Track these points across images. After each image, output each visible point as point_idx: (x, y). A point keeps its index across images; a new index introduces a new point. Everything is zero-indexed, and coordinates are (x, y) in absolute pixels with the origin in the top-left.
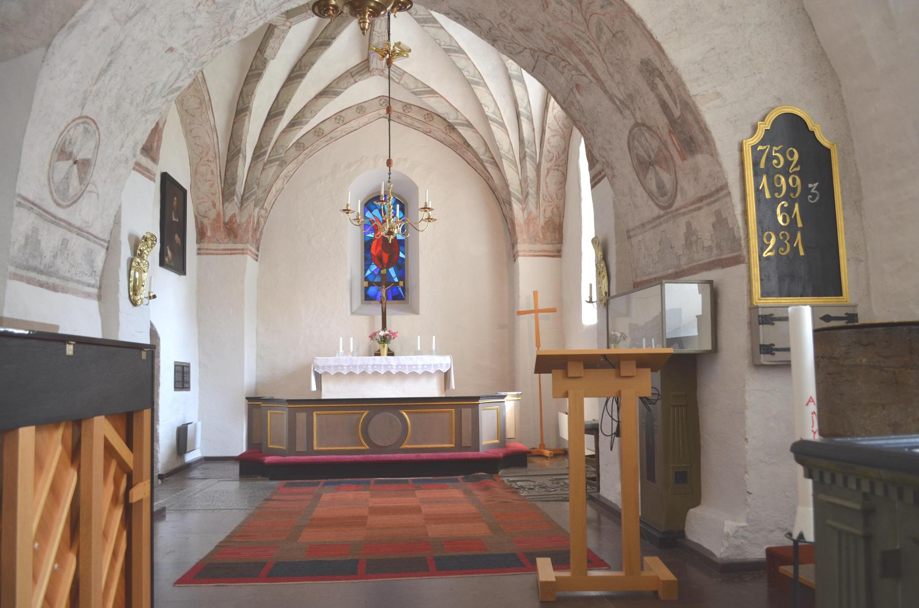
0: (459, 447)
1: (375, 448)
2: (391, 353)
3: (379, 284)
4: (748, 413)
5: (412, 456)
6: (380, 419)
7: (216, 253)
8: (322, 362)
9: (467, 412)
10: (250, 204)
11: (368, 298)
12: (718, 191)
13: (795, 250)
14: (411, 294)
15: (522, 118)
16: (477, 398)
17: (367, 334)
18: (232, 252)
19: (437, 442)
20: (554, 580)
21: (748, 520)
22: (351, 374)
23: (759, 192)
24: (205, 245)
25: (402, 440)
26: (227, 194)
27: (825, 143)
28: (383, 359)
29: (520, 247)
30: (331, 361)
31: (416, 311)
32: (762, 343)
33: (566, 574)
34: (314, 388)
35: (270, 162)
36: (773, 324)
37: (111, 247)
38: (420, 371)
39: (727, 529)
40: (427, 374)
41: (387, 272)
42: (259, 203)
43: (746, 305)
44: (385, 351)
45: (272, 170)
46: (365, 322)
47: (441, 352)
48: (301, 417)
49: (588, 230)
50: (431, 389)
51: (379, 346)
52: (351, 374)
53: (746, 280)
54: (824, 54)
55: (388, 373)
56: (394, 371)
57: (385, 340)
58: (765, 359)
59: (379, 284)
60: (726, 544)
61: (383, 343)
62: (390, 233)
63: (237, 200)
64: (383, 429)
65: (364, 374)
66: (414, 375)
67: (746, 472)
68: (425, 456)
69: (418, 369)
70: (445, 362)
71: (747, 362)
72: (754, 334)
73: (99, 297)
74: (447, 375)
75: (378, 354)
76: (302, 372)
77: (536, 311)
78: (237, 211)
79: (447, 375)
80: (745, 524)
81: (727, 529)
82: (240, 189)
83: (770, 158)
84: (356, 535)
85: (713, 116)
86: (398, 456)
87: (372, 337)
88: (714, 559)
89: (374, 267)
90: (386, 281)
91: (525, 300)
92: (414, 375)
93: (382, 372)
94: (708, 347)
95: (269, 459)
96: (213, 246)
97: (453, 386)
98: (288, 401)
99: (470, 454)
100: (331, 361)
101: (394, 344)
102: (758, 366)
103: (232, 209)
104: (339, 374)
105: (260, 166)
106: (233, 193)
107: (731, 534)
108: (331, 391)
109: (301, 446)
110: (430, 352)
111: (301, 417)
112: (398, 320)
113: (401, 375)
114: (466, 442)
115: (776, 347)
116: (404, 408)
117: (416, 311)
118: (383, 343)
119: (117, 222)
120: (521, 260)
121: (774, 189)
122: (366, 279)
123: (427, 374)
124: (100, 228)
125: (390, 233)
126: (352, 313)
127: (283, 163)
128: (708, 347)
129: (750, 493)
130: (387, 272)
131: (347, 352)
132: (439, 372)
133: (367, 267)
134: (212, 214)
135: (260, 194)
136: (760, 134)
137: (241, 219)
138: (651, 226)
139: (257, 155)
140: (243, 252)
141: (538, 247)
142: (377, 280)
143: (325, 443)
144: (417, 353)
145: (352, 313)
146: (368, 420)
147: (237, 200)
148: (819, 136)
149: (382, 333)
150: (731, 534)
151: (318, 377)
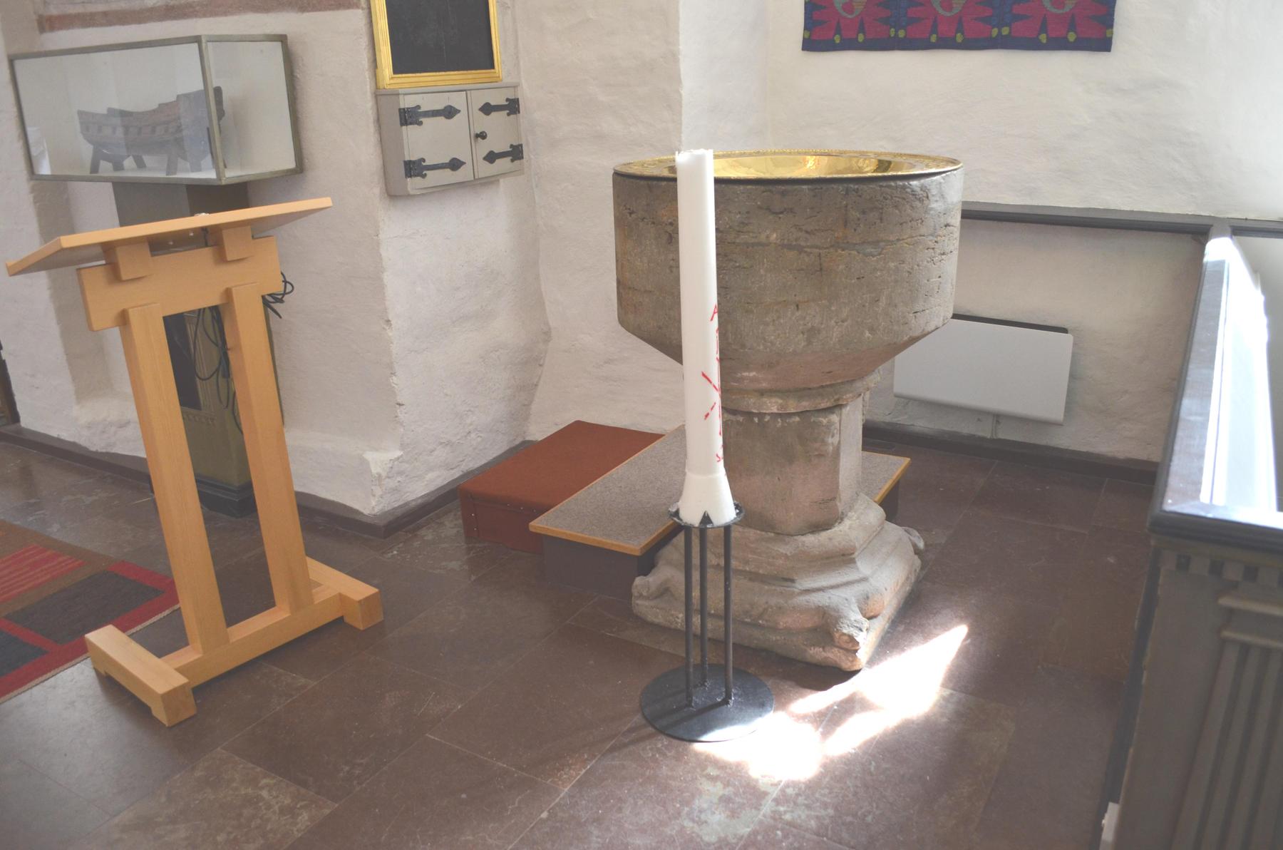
4: (387, 278)
12: (847, 650)
15: (683, 599)
20: (181, 680)
21: (402, 447)
32: (407, 159)
33: (187, 656)
36: (420, 123)
39: (375, 469)
43: (368, 88)
49: (731, 665)
53: (364, 41)
58: (414, 184)
60: (378, 491)
67: (393, 374)
71: (377, 191)
72: (387, 144)
80: (399, 453)
81: (375, 469)
88: (364, 520)
94: (291, 164)
102: (393, 195)
107: (384, 474)
115: (427, 163)
128: (291, 164)
129: (400, 405)
138: (715, 580)
150: (384, 474)
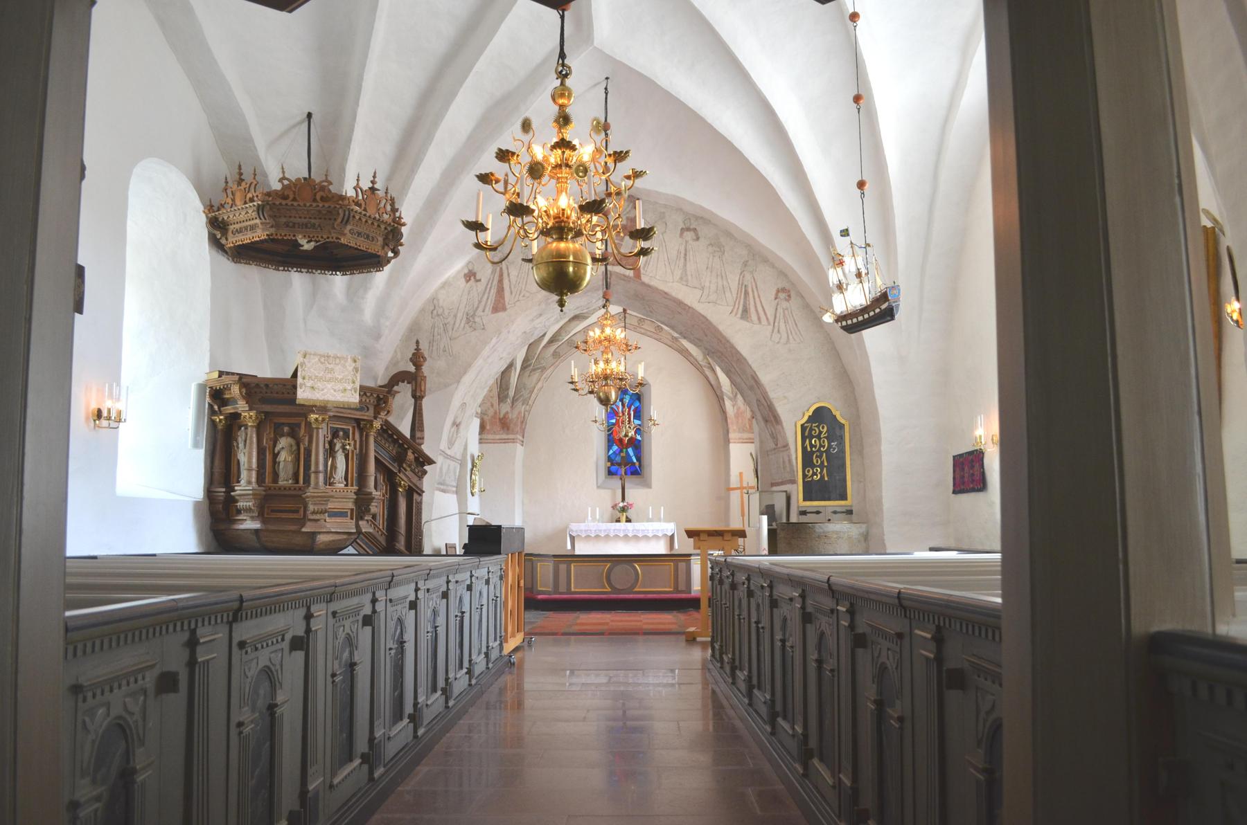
0: (677, 590)
1: (615, 590)
2: (628, 520)
3: (619, 464)
5: (642, 596)
6: (620, 569)
7: (494, 442)
8: (575, 528)
9: (682, 565)
10: (519, 404)
11: (610, 473)
13: (822, 477)
14: (645, 471)
16: (690, 555)
17: (609, 505)
18: (505, 441)
19: (662, 588)
22: (597, 536)
23: (804, 448)
24: (485, 436)
25: (634, 586)
26: (502, 397)
27: (843, 421)
28: (623, 525)
29: (732, 435)
30: (582, 526)
31: (649, 486)
34: (569, 547)
35: (534, 370)
37: (463, 464)
38: (650, 535)
40: (656, 537)
41: (626, 460)
42: (525, 402)
44: (624, 519)
45: (536, 376)
46: (607, 496)
47: (667, 520)
48: (563, 567)
50: (660, 548)
51: (619, 515)
52: (597, 536)
54: (845, 372)
55: (626, 536)
56: (630, 535)
57: (623, 510)
59: (619, 464)
61: (622, 512)
62: (626, 435)
63: (509, 401)
64: (621, 576)
65: (607, 536)
66: (646, 537)
68: (650, 596)
69: (651, 532)
70: (669, 528)
73: (457, 493)
74: (672, 537)
75: (618, 521)
76: (561, 533)
77: (741, 488)
78: (509, 409)
79: (672, 537)
82: (511, 393)
83: (811, 430)
84: (606, 627)
85: (782, 409)
86: (631, 596)
87: (614, 507)
89: (615, 448)
90: (627, 461)
91: (734, 481)
92: (646, 537)
93: (622, 535)
95: (540, 597)
96: (490, 436)
97: (676, 546)
98: (555, 556)
99: (684, 596)
100: (582, 526)
101: (631, 513)
103: (505, 408)
104: (588, 537)
105: (527, 373)
106: (507, 396)
108: (582, 549)
109: (562, 588)
110: (660, 520)
111: (563, 567)
112: (635, 494)
113: (636, 537)
114: (682, 587)
116: (636, 561)
117: (649, 486)
118: (622, 512)
119: (465, 449)
120: (731, 445)
121: (812, 446)
122: (609, 459)
123: (656, 537)
124: (459, 456)
125: (626, 435)
126: (598, 487)
127: (544, 369)
130: (626, 460)
131: (594, 519)
132: (665, 535)
133: (609, 448)
134: (491, 412)
135: (526, 396)
136: (806, 418)
137: (513, 416)
139: (524, 368)
140: (514, 441)
141: (746, 435)
142: (618, 459)
143: (579, 587)
144: (649, 520)
145: (598, 487)
146: (610, 571)
147: (509, 401)
148: (839, 418)
149: (621, 505)
151: (573, 538)
